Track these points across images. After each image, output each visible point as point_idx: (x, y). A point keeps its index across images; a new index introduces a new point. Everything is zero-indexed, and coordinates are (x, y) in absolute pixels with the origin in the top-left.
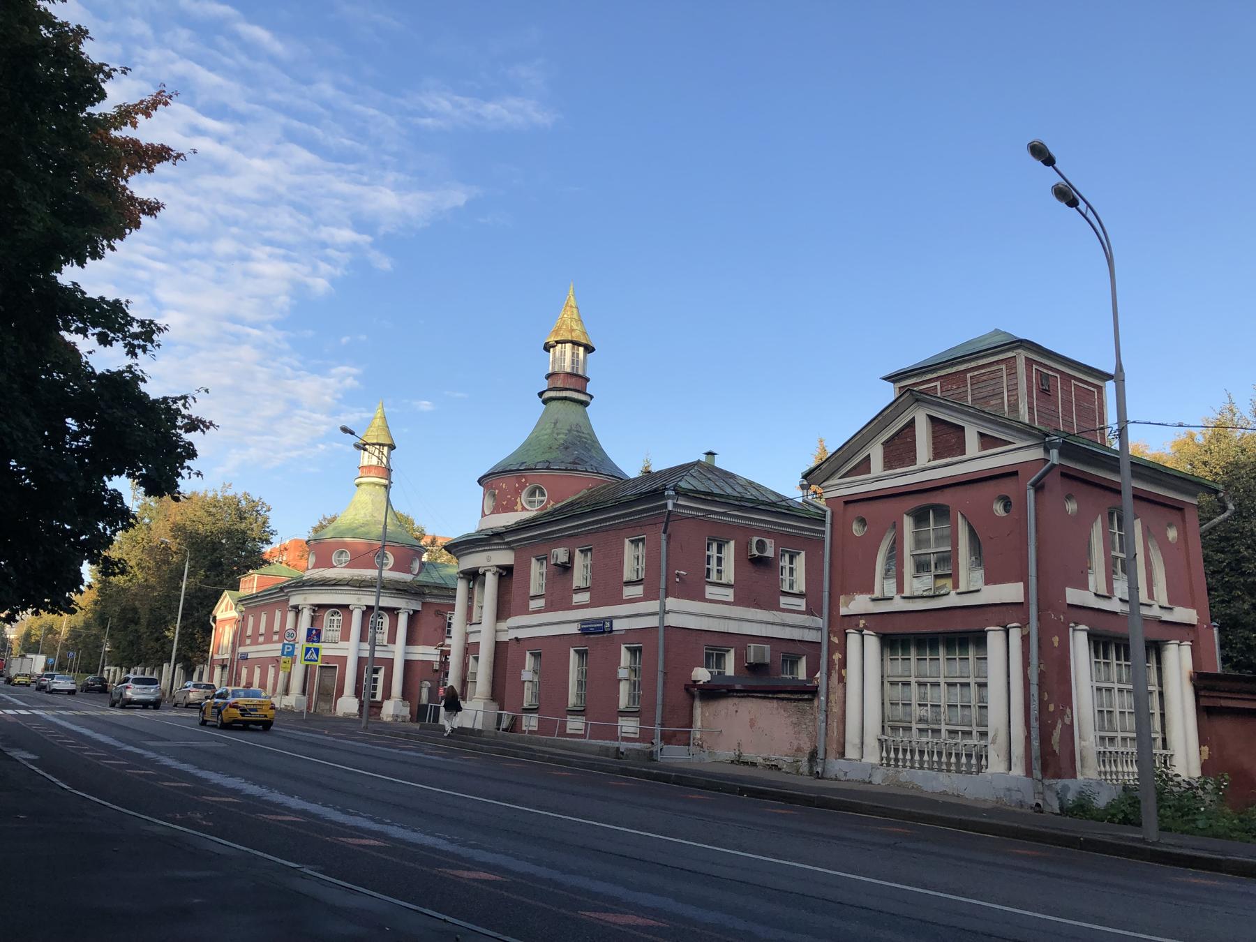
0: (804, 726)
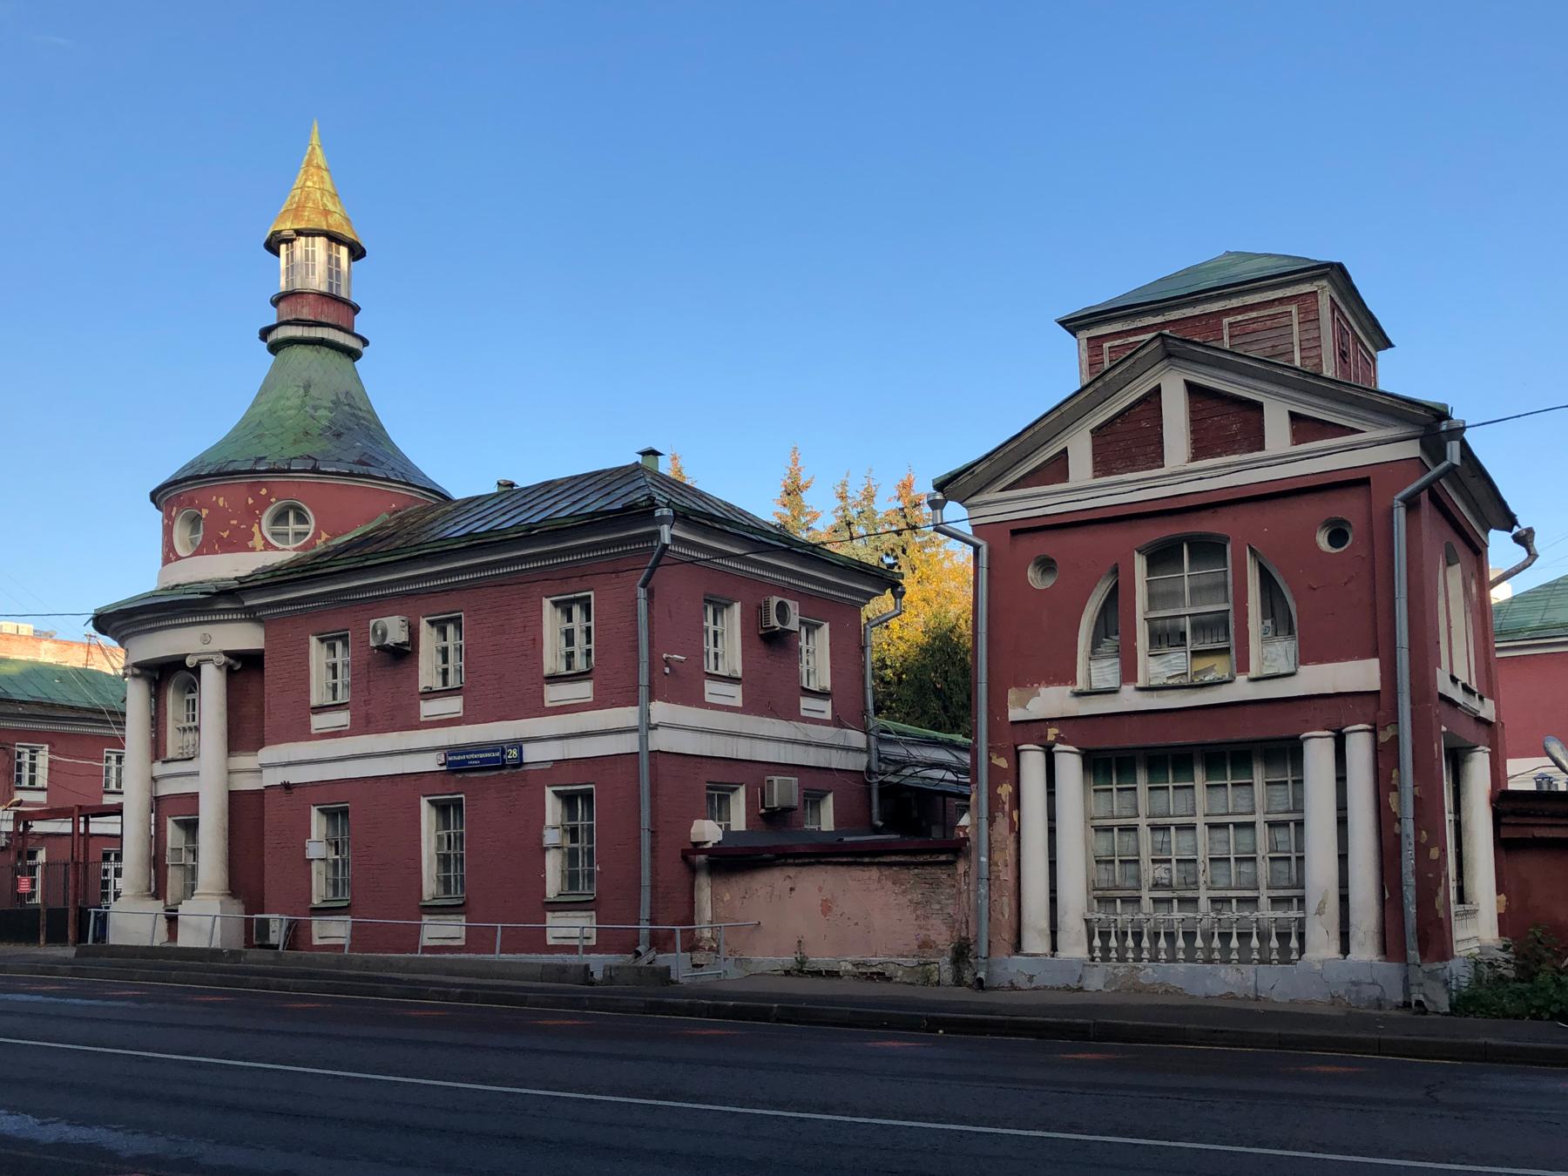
0: (938, 907)
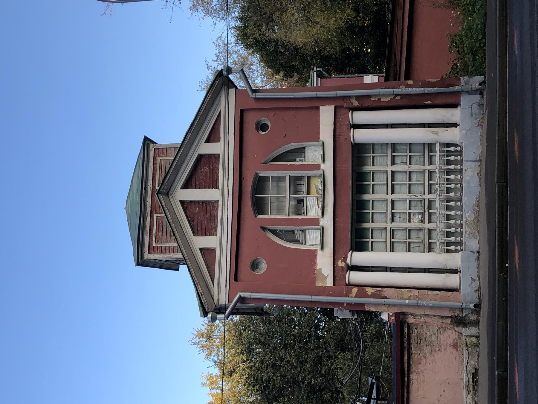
0: (433, 336)
